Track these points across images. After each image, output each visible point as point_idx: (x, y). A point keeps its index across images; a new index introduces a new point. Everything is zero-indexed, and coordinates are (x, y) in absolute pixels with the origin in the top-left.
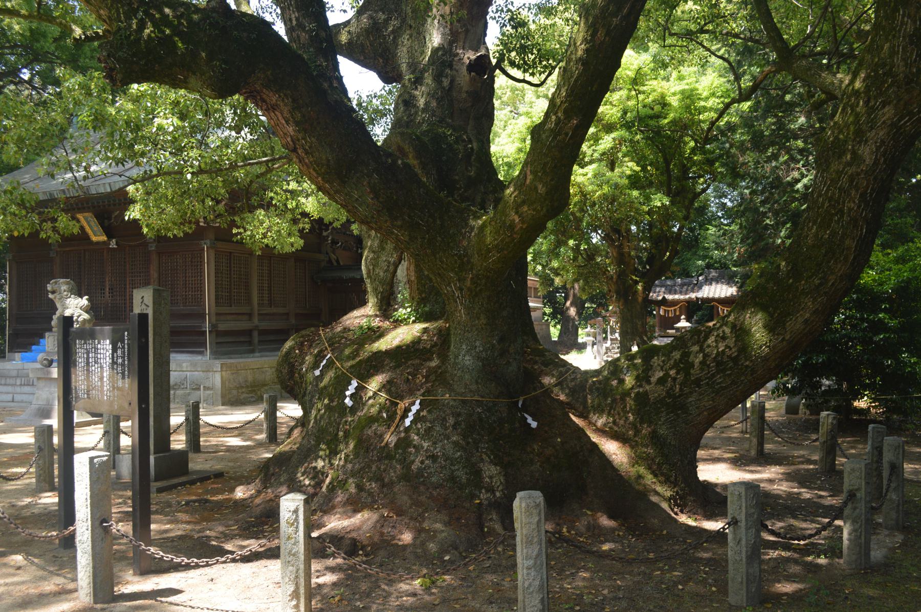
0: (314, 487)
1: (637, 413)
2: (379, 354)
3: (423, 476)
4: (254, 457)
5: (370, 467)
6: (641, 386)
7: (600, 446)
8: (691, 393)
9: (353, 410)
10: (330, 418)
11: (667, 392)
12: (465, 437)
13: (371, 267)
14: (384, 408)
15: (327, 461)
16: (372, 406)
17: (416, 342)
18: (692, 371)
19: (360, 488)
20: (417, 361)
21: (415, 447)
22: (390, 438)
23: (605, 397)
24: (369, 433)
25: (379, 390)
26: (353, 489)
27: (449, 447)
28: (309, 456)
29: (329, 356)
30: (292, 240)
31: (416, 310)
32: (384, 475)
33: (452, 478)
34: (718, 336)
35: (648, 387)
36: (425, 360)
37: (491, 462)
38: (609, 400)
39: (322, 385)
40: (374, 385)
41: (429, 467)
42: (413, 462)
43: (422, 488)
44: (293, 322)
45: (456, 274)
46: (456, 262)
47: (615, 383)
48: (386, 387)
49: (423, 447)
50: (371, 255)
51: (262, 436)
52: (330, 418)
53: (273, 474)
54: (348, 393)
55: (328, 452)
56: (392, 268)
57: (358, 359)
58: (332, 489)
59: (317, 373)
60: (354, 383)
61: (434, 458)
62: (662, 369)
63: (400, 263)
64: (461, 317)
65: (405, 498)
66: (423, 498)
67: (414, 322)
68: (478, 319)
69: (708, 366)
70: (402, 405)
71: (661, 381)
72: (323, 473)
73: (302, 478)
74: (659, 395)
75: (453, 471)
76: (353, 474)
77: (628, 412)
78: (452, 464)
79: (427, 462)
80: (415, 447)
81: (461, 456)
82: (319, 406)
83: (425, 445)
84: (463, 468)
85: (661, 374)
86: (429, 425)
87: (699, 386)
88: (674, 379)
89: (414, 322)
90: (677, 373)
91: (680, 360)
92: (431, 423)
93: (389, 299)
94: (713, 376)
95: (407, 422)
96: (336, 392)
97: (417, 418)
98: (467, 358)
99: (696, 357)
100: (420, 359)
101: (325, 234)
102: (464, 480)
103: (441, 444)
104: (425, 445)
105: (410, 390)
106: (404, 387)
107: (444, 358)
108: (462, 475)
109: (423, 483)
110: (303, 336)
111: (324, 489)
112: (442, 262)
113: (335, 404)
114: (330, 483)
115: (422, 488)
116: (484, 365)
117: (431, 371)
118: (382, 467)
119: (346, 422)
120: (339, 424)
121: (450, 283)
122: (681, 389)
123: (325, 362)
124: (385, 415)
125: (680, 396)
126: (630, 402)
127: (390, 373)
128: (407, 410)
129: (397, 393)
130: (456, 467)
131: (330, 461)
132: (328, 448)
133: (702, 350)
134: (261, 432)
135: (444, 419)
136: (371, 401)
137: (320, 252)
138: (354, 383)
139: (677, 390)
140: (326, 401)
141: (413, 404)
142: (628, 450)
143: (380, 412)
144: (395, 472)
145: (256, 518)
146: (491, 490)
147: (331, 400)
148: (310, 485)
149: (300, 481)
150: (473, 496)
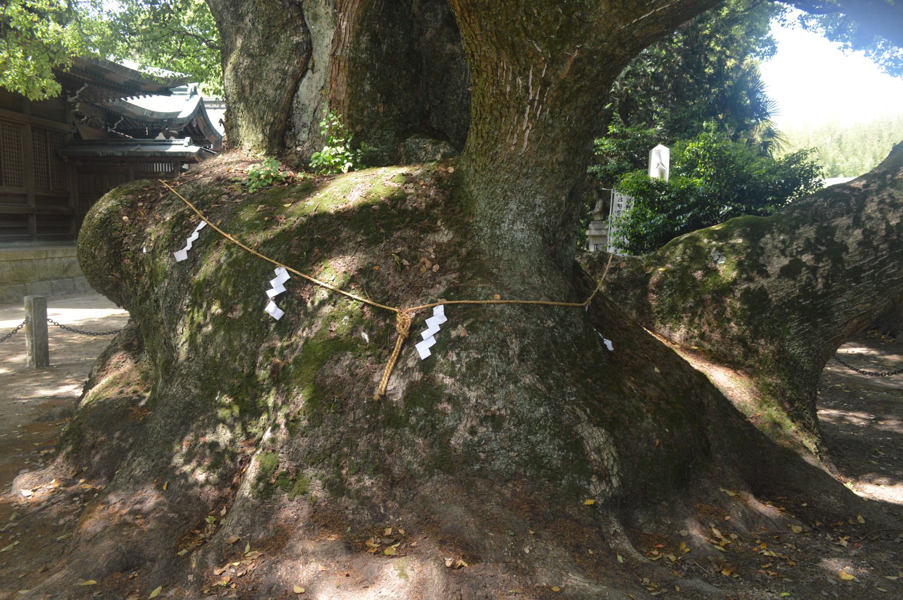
0: (219, 486)
1: (747, 319)
2: (320, 219)
3: (478, 459)
4: (22, 398)
5: (353, 445)
6: (750, 279)
7: (708, 376)
8: (842, 291)
9: (285, 327)
10: (230, 342)
11: (803, 289)
12: (542, 378)
13: (247, 82)
14: (361, 322)
15: (238, 430)
16: (333, 318)
17: (396, 201)
18: (845, 257)
19: (336, 488)
20: (409, 233)
21: (450, 399)
22: (389, 383)
23: (684, 297)
24: (338, 371)
25: (345, 287)
26: (318, 491)
27: (520, 397)
28: (193, 419)
29: (202, 225)
30: (44, 83)
31: (353, 149)
32: (389, 460)
33: (535, 460)
34: (882, 201)
35: (764, 282)
36: (425, 231)
37: (590, 421)
38: (690, 302)
39: (199, 277)
40: (332, 273)
41: (488, 441)
42: (453, 430)
43: (481, 485)
44: (33, 206)
45: (550, 46)
46: (556, 20)
47: (698, 274)
48: (361, 278)
49: (467, 400)
50: (246, 62)
51: (23, 358)
52: (230, 342)
53: (93, 447)
54: (271, 293)
55: (236, 410)
56: (289, 83)
57: (278, 229)
58: (267, 486)
59: (181, 255)
60: (282, 275)
61: (495, 421)
62: (783, 252)
63: (303, 75)
64: (519, 145)
65: (458, 510)
66: (492, 507)
67: (351, 170)
68: (553, 150)
69: (876, 249)
70: (406, 315)
71: (787, 272)
72: (233, 456)
73: (187, 468)
74: (788, 294)
75: (534, 445)
76: (314, 458)
77: (729, 320)
78: (530, 432)
79: (482, 430)
80: (450, 399)
81: (546, 414)
82: (198, 317)
83: (472, 395)
84: (553, 437)
85: (785, 261)
86: (474, 355)
87: (858, 280)
88: (814, 270)
89: (351, 170)
90: (818, 259)
91: (817, 240)
92: (479, 351)
93: (283, 136)
94: (883, 263)
95: (423, 350)
96: (235, 292)
97: (443, 342)
98: (519, 226)
99: (848, 235)
100: (414, 228)
101: (70, 100)
102: (557, 462)
103: (502, 392)
104: (472, 395)
105: (411, 286)
106: (396, 280)
107: (463, 229)
108: (551, 450)
109: (481, 474)
110: (131, 192)
111: (246, 490)
112: (529, 15)
113: (237, 314)
114: (259, 479)
115: (481, 485)
116: (545, 241)
117: (443, 255)
118: (383, 443)
119: (272, 350)
120: (255, 355)
121: (527, 69)
122: (826, 285)
123: (195, 236)
124: (365, 336)
125: (824, 295)
126: (734, 303)
127: (360, 255)
128: (418, 326)
129: (384, 293)
130: (539, 437)
131: (244, 429)
132: (236, 401)
133: (857, 223)
134: (17, 351)
135: (503, 344)
136: (327, 309)
137: (65, 121)
138: (282, 275)
139: (820, 286)
140: (216, 309)
141: (430, 313)
142: (745, 379)
143: (354, 330)
144: (415, 453)
145: (100, 576)
146: (604, 476)
147: (227, 307)
148: (207, 481)
149: (185, 475)
150: (578, 493)
